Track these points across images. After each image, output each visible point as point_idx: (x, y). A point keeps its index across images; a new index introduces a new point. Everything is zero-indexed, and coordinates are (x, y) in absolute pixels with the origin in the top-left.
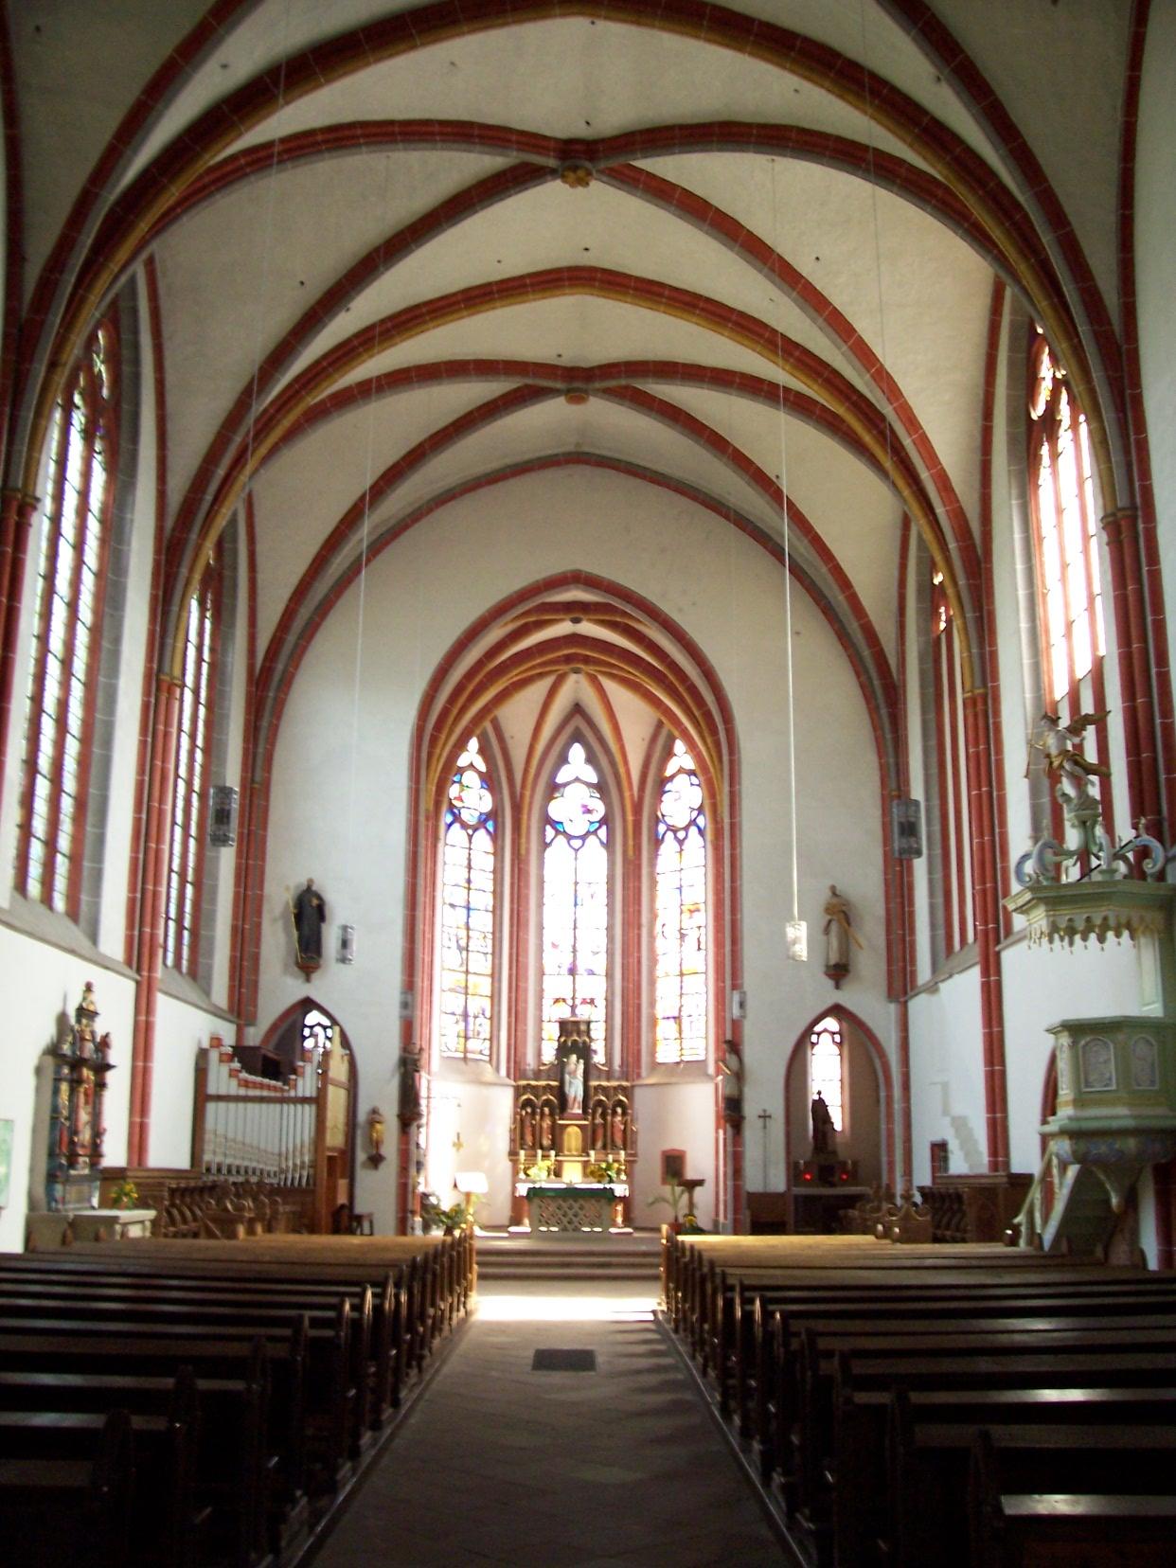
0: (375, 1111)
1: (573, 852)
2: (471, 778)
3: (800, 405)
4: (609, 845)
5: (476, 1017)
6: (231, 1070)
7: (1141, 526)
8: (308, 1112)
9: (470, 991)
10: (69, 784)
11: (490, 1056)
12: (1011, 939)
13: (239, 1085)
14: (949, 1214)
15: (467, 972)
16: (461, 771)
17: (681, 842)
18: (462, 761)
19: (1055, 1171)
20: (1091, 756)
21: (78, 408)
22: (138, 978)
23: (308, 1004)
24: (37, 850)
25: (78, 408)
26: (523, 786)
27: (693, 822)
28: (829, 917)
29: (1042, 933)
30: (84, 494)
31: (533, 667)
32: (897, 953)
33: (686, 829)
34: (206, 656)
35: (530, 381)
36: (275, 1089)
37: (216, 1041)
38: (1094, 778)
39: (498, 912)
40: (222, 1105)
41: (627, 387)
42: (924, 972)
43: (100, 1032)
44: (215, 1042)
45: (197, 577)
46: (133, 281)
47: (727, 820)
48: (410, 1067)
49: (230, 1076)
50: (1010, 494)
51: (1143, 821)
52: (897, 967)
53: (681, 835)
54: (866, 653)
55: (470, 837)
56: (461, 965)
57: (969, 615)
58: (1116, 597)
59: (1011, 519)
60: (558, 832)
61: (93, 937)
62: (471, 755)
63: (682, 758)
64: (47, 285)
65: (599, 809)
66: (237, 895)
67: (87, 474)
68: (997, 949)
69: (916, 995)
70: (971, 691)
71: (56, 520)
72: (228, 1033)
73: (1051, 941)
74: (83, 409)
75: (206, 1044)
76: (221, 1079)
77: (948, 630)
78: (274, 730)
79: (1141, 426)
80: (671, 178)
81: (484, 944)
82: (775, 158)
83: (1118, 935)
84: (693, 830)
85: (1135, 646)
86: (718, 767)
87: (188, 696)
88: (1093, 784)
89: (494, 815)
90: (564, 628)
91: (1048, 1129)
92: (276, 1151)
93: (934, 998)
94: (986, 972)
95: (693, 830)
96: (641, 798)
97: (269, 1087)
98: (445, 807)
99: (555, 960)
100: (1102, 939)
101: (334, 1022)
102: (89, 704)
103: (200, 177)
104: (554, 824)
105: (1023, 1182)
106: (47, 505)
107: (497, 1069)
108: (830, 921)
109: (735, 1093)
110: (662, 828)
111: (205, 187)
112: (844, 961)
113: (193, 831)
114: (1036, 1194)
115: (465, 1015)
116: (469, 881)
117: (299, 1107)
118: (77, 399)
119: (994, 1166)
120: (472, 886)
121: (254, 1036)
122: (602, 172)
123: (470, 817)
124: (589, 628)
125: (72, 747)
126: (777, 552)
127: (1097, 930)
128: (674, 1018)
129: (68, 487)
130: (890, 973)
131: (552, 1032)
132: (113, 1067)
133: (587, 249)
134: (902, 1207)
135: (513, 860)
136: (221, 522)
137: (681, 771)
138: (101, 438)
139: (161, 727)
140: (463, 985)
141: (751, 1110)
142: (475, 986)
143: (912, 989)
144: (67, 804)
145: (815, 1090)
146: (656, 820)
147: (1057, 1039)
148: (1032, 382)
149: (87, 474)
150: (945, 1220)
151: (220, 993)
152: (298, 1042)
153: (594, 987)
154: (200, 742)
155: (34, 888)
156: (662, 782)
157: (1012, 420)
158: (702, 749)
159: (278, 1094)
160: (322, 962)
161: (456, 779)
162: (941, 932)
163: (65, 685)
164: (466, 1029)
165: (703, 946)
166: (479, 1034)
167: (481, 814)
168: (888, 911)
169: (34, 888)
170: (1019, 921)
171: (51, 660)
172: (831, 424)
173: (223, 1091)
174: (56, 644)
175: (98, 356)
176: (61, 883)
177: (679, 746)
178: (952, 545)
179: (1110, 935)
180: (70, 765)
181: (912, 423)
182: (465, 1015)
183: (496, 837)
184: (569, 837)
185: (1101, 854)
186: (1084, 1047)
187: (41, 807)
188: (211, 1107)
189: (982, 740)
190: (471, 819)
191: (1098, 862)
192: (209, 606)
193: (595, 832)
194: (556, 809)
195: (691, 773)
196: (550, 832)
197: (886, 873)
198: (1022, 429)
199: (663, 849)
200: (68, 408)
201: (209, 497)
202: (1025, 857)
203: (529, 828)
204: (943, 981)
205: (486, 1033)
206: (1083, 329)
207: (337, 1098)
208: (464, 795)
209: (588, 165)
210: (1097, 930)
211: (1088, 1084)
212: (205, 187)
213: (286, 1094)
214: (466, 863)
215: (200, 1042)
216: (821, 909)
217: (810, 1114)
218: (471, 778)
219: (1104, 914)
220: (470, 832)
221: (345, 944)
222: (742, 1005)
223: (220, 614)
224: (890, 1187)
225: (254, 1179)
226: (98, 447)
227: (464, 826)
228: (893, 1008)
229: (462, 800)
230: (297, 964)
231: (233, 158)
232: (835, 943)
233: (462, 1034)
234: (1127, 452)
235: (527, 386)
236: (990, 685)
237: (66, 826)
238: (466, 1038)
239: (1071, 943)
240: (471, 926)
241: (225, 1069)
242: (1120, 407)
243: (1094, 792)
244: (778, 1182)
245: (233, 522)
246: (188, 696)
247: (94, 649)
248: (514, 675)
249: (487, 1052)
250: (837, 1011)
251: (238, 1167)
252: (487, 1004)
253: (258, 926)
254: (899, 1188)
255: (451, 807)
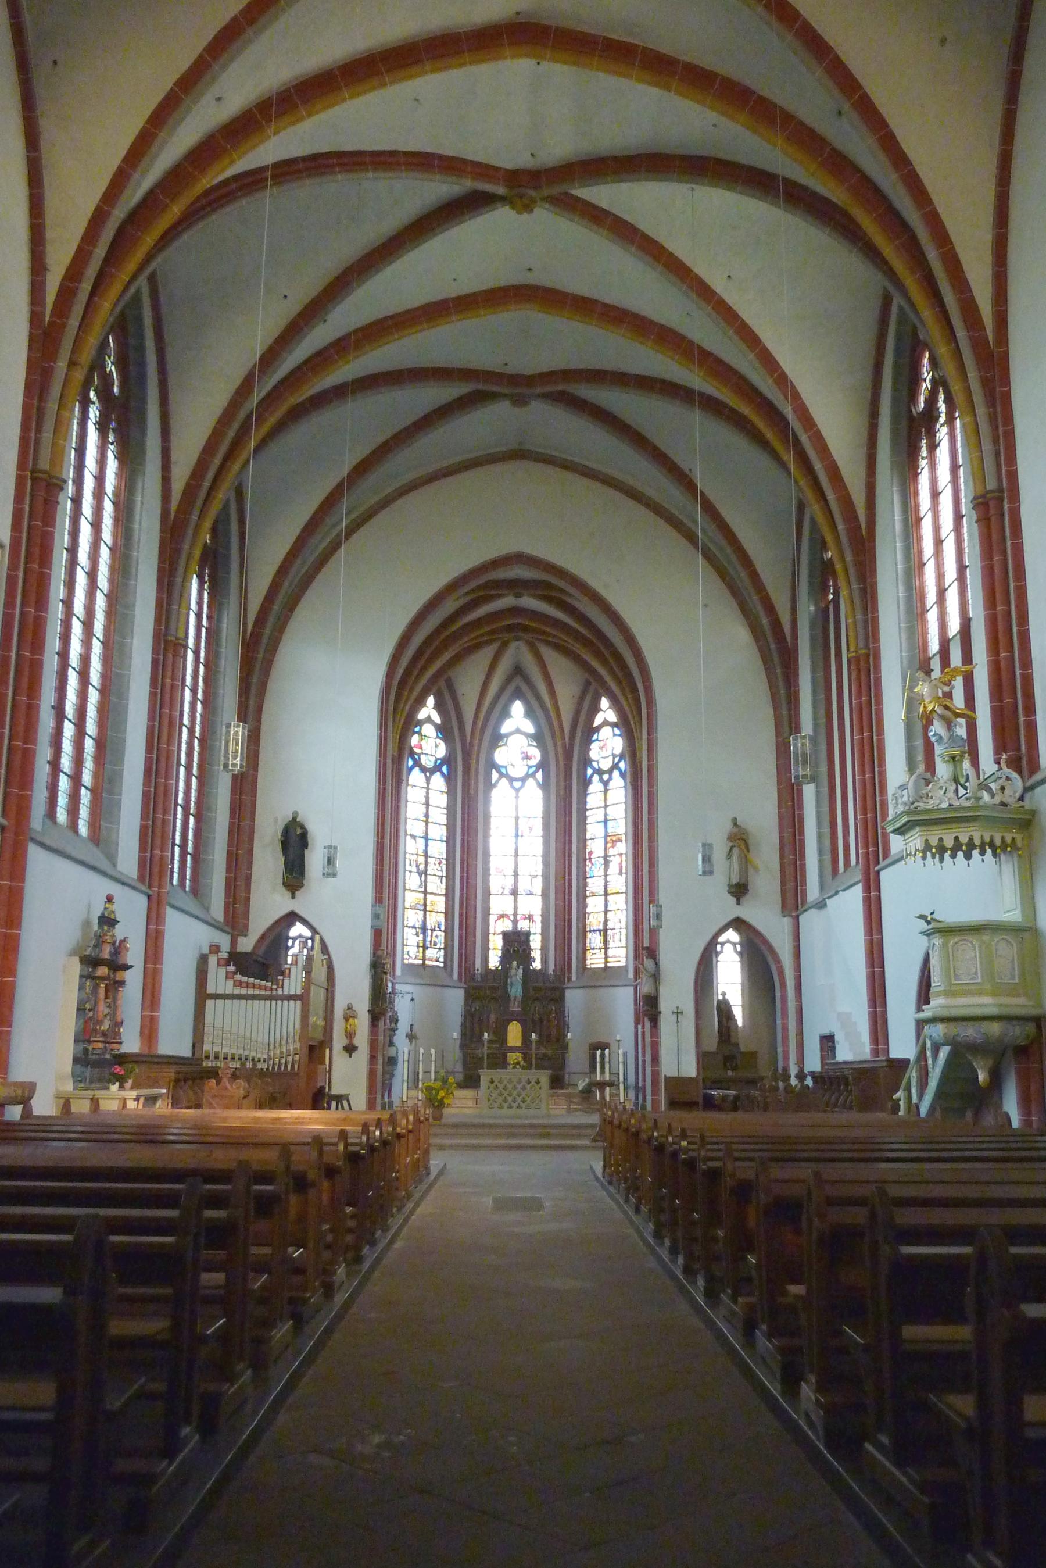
0: (350, 1008)
1: (513, 792)
2: (428, 730)
3: (712, 406)
4: (545, 786)
5: (433, 930)
6: (227, 973)
7: (1006, 506)
8: (296, 1007)
9: (428, 908)
10: (91, 728)
11: (445, 962)
12: (888, 861)
13: (235, 985)
14: (836, 1094)
15: (425, 893)
16: (420, 723)
17: (606, 784)
18: (422, 715)
19: (929, 1054)
20: (959, 701)
21: (93, 403)
22: (150, 893)
23: (292, 917)
24: (64, 783)
25: (93, 403)
26: (472, 737)
27: (615, 766)
28: (731, 844)
29: (916, 850)
30: (100, 479)
31: (482, 635)
32: (789, 871)
33: (610, 771)
34: (205, 622)
35: (481, 386)
36: (266, 988)
37: (215, 949)
38: (962, 721)
39: (451, 842)
40: (220, 1002)
41: (563, 393)
42: (813, 892)
43: (119, 937)
44: (214, 949)
45: (197, 553)
46: (138, 291)
47: (645, 764)
48: (379, 970)
49: (227, 978)
50: (892, 484)
51: (1004, 756)
52: (790, 885)
53: (606, 777)
54: (765, 621)
55: (428, 780)
56: (420, 886)
57: (854, 586)
58: (983, 568)
59: (892, 504)
60: (502, 775)
61: (112, 858)
62: (428, 710)
63: (606, 712)
64: (66, 293)
65: (536, 754)
66: (231, 825)
67: (102, 462)
68: (876, 869)
69: (806, 910)
70: (856, 652)
71: (77, 501)
72: (224, 941)
73: (924, 858)
74: (97, 404)
75: (206, 951)
76: (219, 980)
77: (836, 601)
78: (263, 685)
79: (1009, 418)
80: (604, 205)
81: (440, 869)
82: (694, 186)
83: (983, 853)
84: (616, 773)
85: (999, 608)
86: (637, 718)
87: (190, 656)
88: (961, 726)
89: (448, 760)
90: (507, 601)
91: (922, 1015)
92: (266, 1041)
93: (823, 912)
94: (867, 889)
95: (616, 773)
96: (572, 745)
97: (260, 987)
98: (406, 753)
99: (498, 881)
100: (968, 856)
101: (314, 931)
102: (107, 660)
103: (198, 198)
104: (498, 768)
105: (900, 1066)
106: (70, 489)
107: (451, 975)
108: (732, 848)
109: (653, 992)
110: (589, 771)
111: (203, 208)
112: (743, 881)
113: (195, 771)
114: (913, 1074)
115: (424, 929)
116: (427, 816)
117: (286, 1002)
118: (92, 394)
119: (875, 1052)
120: (430, 820)
121: (246, 944)
122: (545, 199)
123: (428, 762)
124: (529, 602)
125: (93, 696)
126: (691, 537)
127: (964, 848)
128: (600, 931)
129: (87, 473)
130: (783, 892)
131: (496, 943)
132: (132, 966)
133: (530, 269)
134: (796, 1086)
135: (463, 799)
136: (215, 507)
137: (606, 723)
138: (114, 430)
139: (168, 681)
140: (422, 902)
141: (665, 1006)
142: (432, 904)
143: (803, 905)
144: (89, 745)
145: (720, 992)
146: (586, 761)
147: (929, 940)
148: (915, 380)
149: (102, 462)
150: (833, 1099)
151: (217, 910)
152: (283, 952)
153: (532, 905)
154: (200, 696)
155: (62, 816)
156: (590, 731)
157: (895, 419)
158: (624, 704)
159: (268, 993)
160: (304, 882)
161: (417, 729)
162: (828, 857)
163: (87, 644)
164: (424, 940)
165: (624, 871)
166: (435, 944)
167: (437, 760)
168: (781, 839)
169: (62, 816)
170: (896, 844)
171: (75, 621)
172: (739, 422)
173: (220, 991)
174: (79, 607)
175: (110, 358)
176: (84, 812)
177: (604, 703)
178: (841, 527)
179: (975, 853)
180: (92, 712)
181: (808, 422)
182: (424, 929)
183: (449, 779)
184: (511, 780)
185: (967, 784)
186: (953, 946)
187: (67, 746)
188: (210, 1003)
189: (864, 692)
190: (428, 763)
191: (965, 792)
192: (206, 579)
193: (533, 775)
194: (500, 756)
195: (614, 725)
196: (495, 775)
197: (780, 807)
198: (904, 423)
199: (591, 789)
200: (86, 403)
201: (207, 484)
202: (903, 787)
203: (477, 770)
204: (829, 898)
205: (441, 907)
206: (961, 334)
207: (317, 996)
208: (423, 743)
209: (532, 193)
210: (964, 848)
211: (956, 977)
212: (203, 208)
213: (274, 993)
214: (423, 800)
215: (200, 948)
216: (726, 836)
217: (716, 1012)
218: (428, 730)
219: (969, 834)
220: (428, 774)
221: (330, 861)
222: (658, 917)
223: (217, 588)
224: (786, 1070)
225: (249, 1065)
226: (111, 438)
227: (424, 770)
228: (787, 922)
229: (421, 748)
230: (285, 884)
231: (225, 183)
232: (736, 866)
233: (421, 944)
234: (996, 441)
235: (478, 391)
236: (871, 646)
237: (89, 764)
238: (425, 948)
239: (942, 860)
240: (429, 854)
241: (222, 971)
242: (991, 400)
243: (962, 731)
244: (690, 1069)
245: (226, 507)
246: (190, 656)
247: (110, 613)
248: (464, 642)
249: (441, 959)
250: (738, 924)
251: (233, 1055)
252: (441, 918)
253: (250, 852)
254: (793, 1071)
255: (412, 754)
